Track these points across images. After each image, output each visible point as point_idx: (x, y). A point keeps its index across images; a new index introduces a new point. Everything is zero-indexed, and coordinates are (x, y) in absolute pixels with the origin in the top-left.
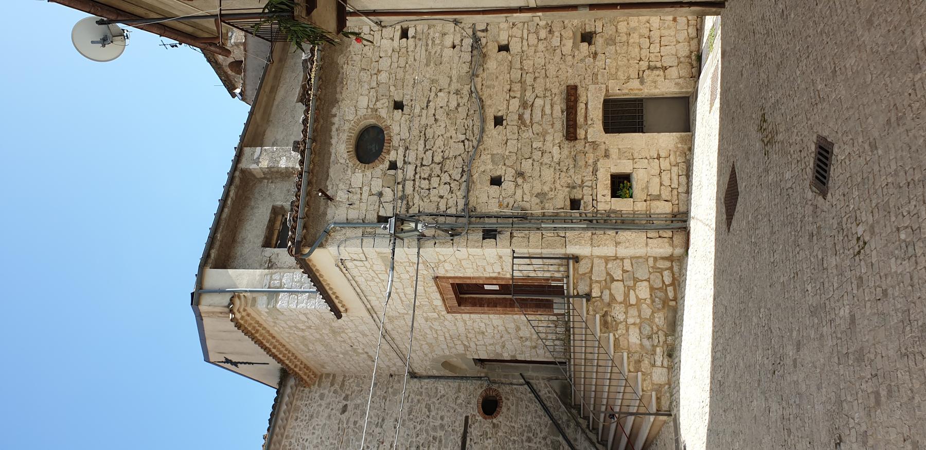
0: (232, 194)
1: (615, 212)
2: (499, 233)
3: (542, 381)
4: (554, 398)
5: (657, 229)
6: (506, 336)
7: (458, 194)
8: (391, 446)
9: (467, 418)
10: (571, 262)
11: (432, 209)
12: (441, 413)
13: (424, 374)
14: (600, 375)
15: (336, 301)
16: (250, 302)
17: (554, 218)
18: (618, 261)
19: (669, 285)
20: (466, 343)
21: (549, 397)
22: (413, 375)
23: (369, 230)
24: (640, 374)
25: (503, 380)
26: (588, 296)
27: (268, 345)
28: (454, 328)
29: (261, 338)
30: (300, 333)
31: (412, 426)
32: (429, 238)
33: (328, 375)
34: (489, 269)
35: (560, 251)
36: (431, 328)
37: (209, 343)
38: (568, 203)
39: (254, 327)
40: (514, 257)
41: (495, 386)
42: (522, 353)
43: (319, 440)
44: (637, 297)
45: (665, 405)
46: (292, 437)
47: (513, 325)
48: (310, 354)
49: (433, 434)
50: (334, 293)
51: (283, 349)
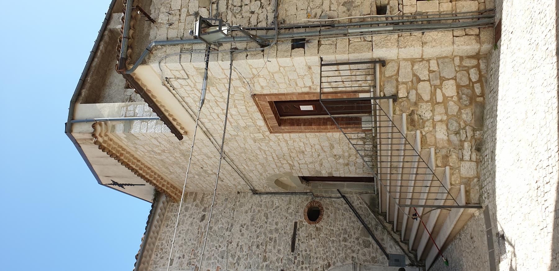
0: (101, 47)
1: (421, 14)
2: (308, 42)
3: (355, 195)
4: (365, 208)
5: (464, 27)
6: (323, 155)
7: (268, 8)
8: (237, 245)
9: (296, 223)
10: (378, 66)
11: (245, 24)
12: (275, 220)
13: (263, 191)
14: (404, 183)
15: (174, 123)
16: (110, 129)
17: (362, 23)
18: (424, 62)
19: (476, 82)
20: (291, 163)
21: (360, 207)
22: (255, 192)
23: (186, 47)
24: (448, 168)
25: (324, 195)
26: (395, 97)
27: (134, 167)
28: (279, 148)
29: (126, 161)
30: (158, 157)
31: (254, 230)
32: (241, 51)
33: (191, 193)
34: (300, 84)
35: (367, 55)
36: (260, 149)
37: (95, 167)
38: (374, 9)
39: (118, 151)
40: (322, 65)
41: (317, 200)
42: (337, 170)
43: (183, 242)
44: (444, 95)
45: (474, 197)
46: (163, 239)
47: (326, 144)
48: (172, 176)
49: (269, 235)
50: (171, 116)
51: (149, 171)
